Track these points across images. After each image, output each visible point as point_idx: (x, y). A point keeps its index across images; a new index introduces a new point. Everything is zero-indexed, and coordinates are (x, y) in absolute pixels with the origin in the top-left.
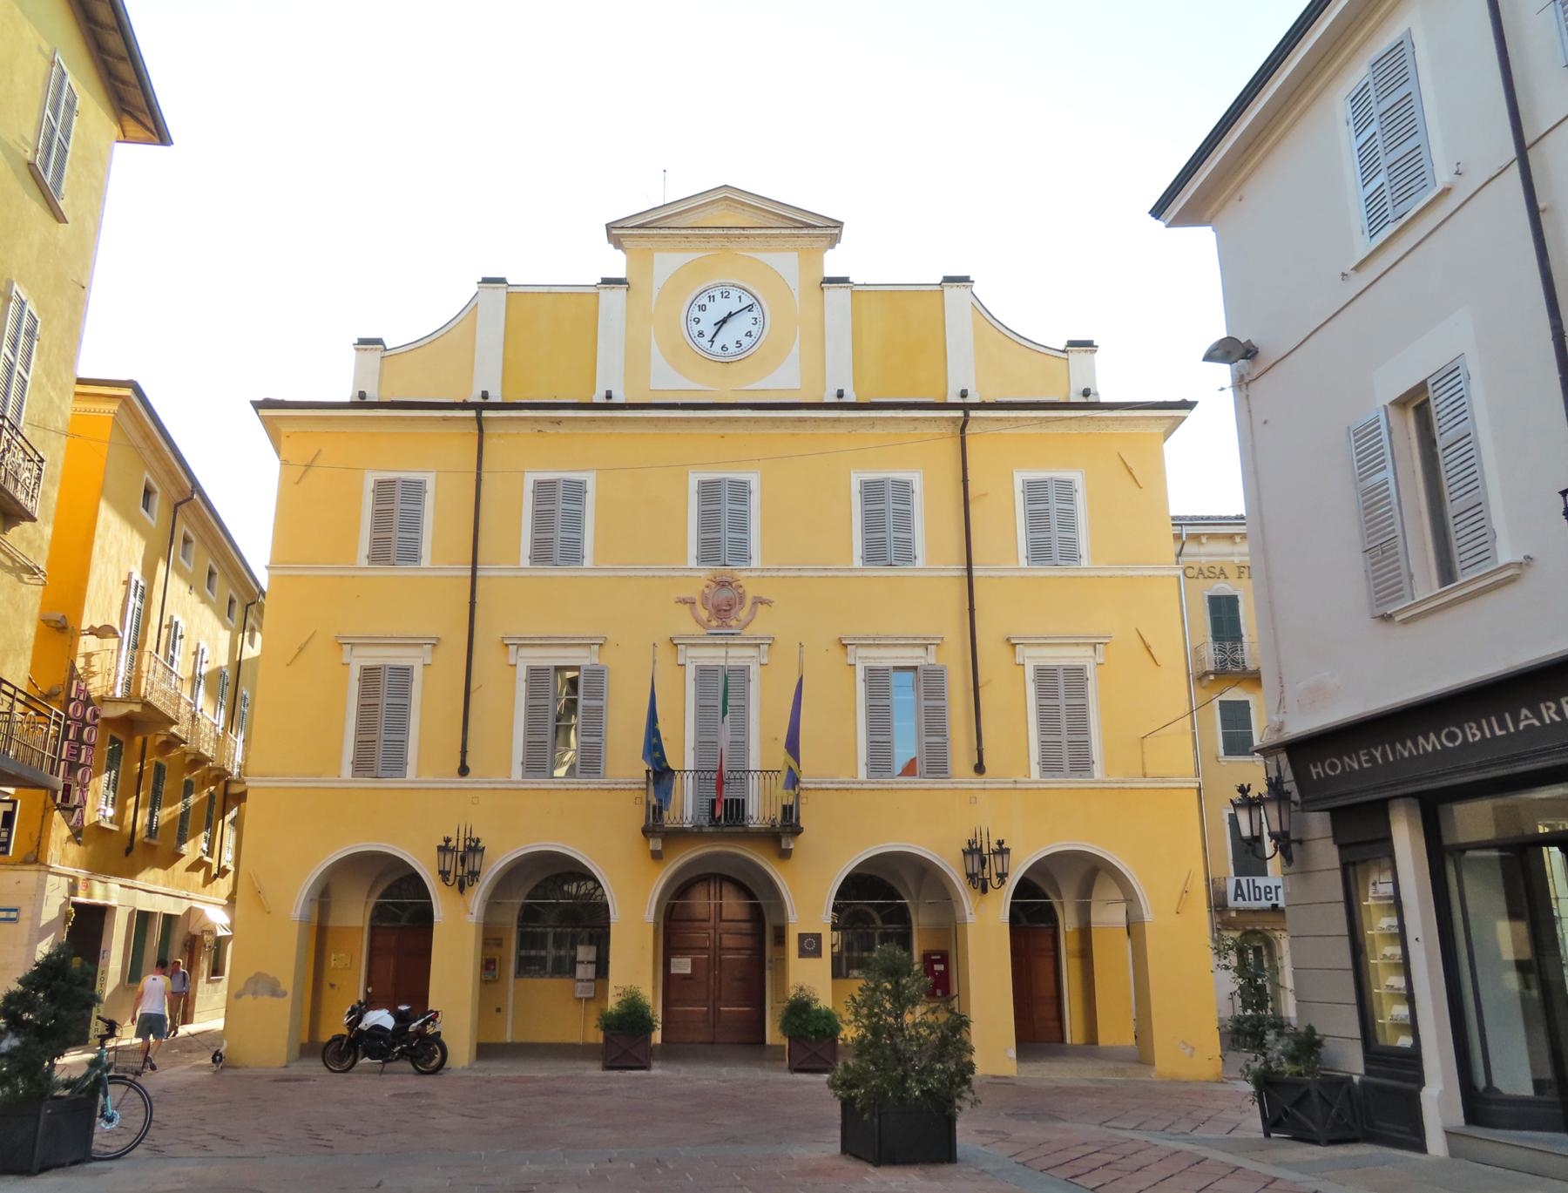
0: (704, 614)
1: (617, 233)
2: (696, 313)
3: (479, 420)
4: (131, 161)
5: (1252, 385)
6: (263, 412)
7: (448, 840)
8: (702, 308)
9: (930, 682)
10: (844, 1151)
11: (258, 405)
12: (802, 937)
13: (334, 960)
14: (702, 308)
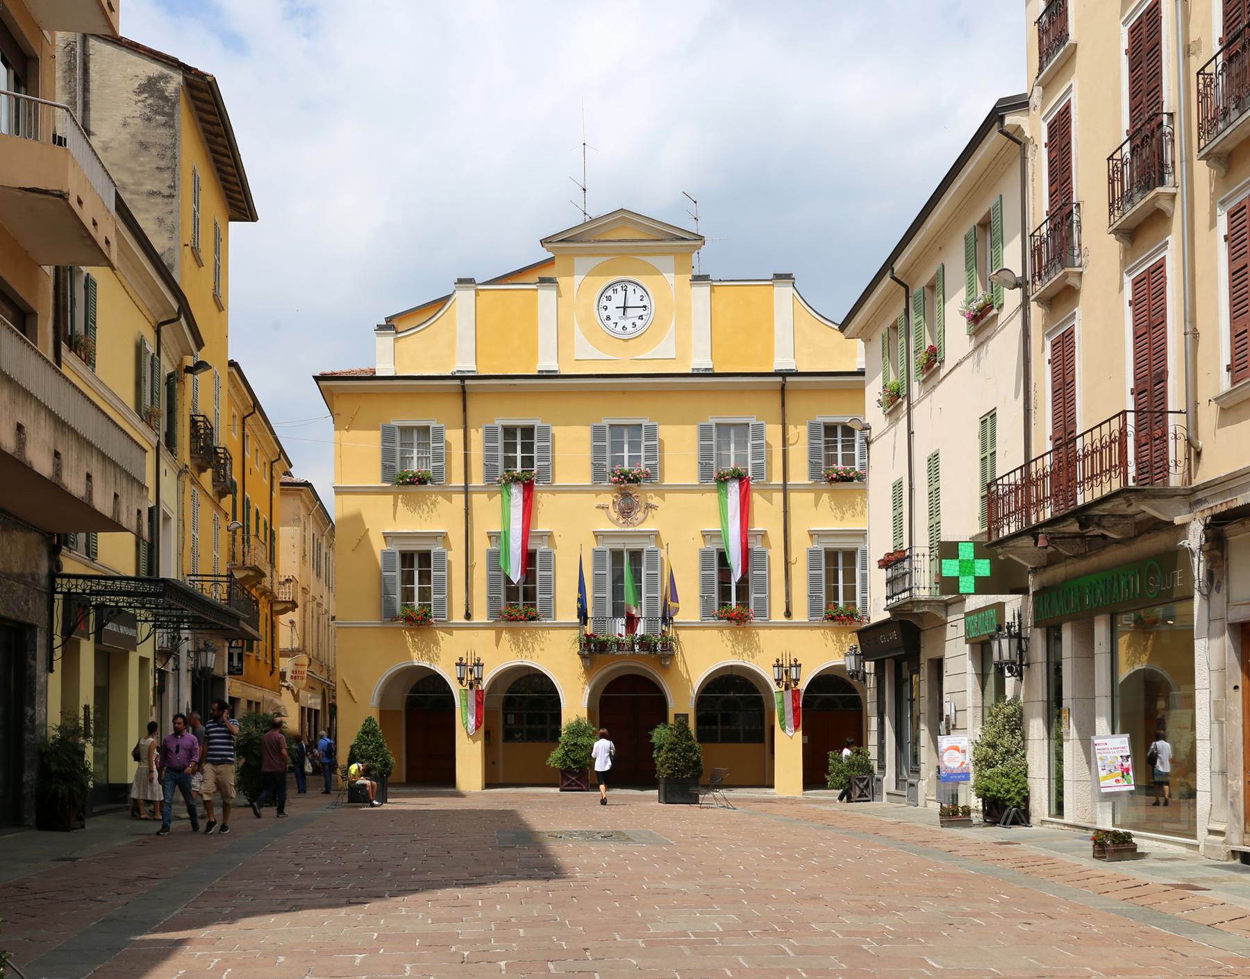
0: (615, 516)
1: (544, 242)
2: (604, 302)
3: (463, 387)
4: (236, 229)
5: (251, 810)
6: (321, 383)
7: (461, 659)
8: (609, 298)
9: (316, 711)
10: (338, 427)
11: (317, 379)
12: (677, 716)
13: (792, 450)
14: (609, 298)
